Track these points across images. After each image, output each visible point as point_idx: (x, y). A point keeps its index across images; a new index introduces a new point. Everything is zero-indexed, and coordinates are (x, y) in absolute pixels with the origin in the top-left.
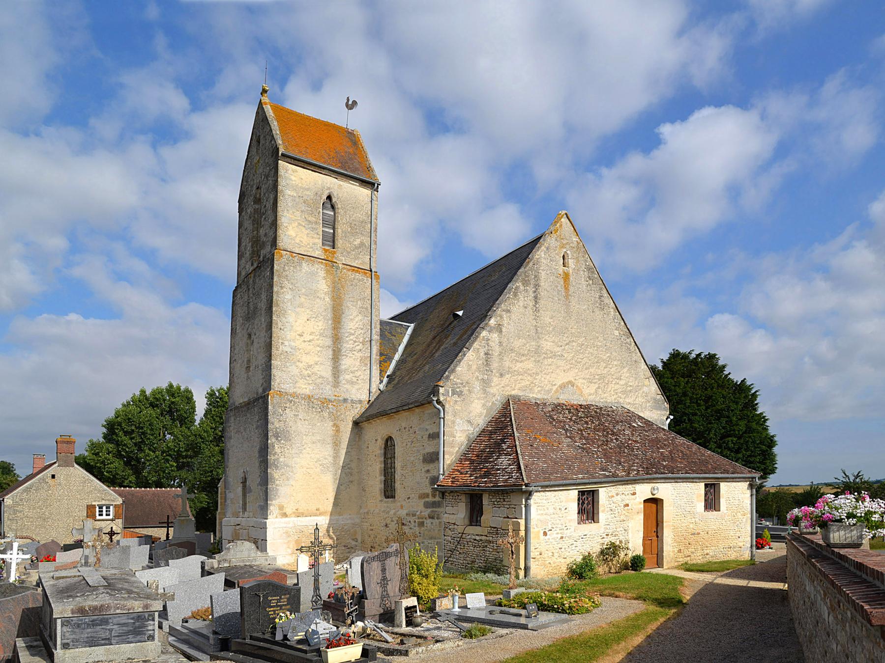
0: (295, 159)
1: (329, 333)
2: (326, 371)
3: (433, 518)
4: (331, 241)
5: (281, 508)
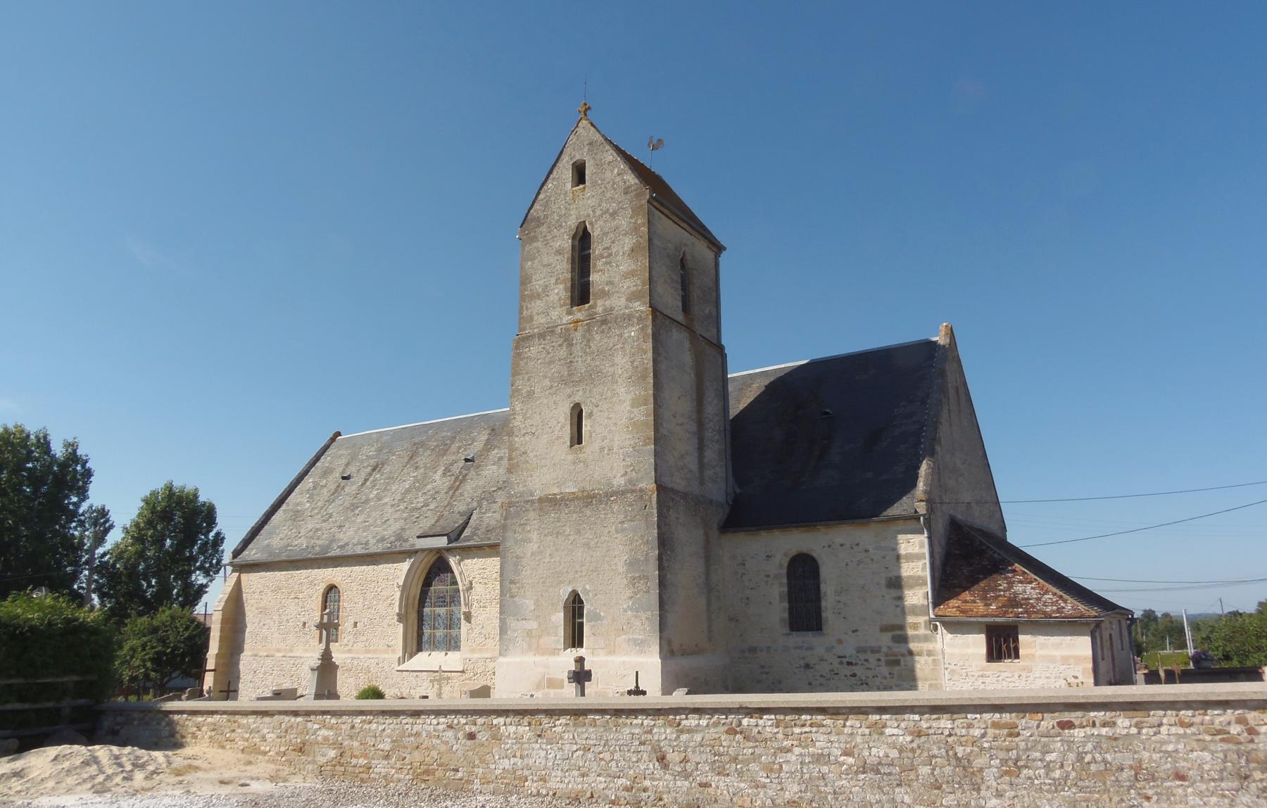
4: (686, 308)
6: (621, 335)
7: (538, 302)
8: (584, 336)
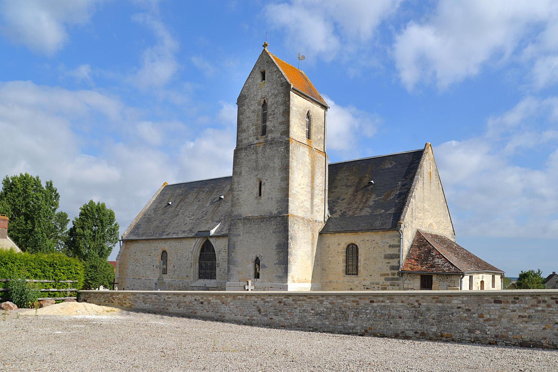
0: (297, 91)
1: (310, 184)
2: (308, 204)
3: (394, 285)
4: (309, 136)
5: (293, 278)
6: (277, 150)
7: (245, 133)
8: (263, 150)
